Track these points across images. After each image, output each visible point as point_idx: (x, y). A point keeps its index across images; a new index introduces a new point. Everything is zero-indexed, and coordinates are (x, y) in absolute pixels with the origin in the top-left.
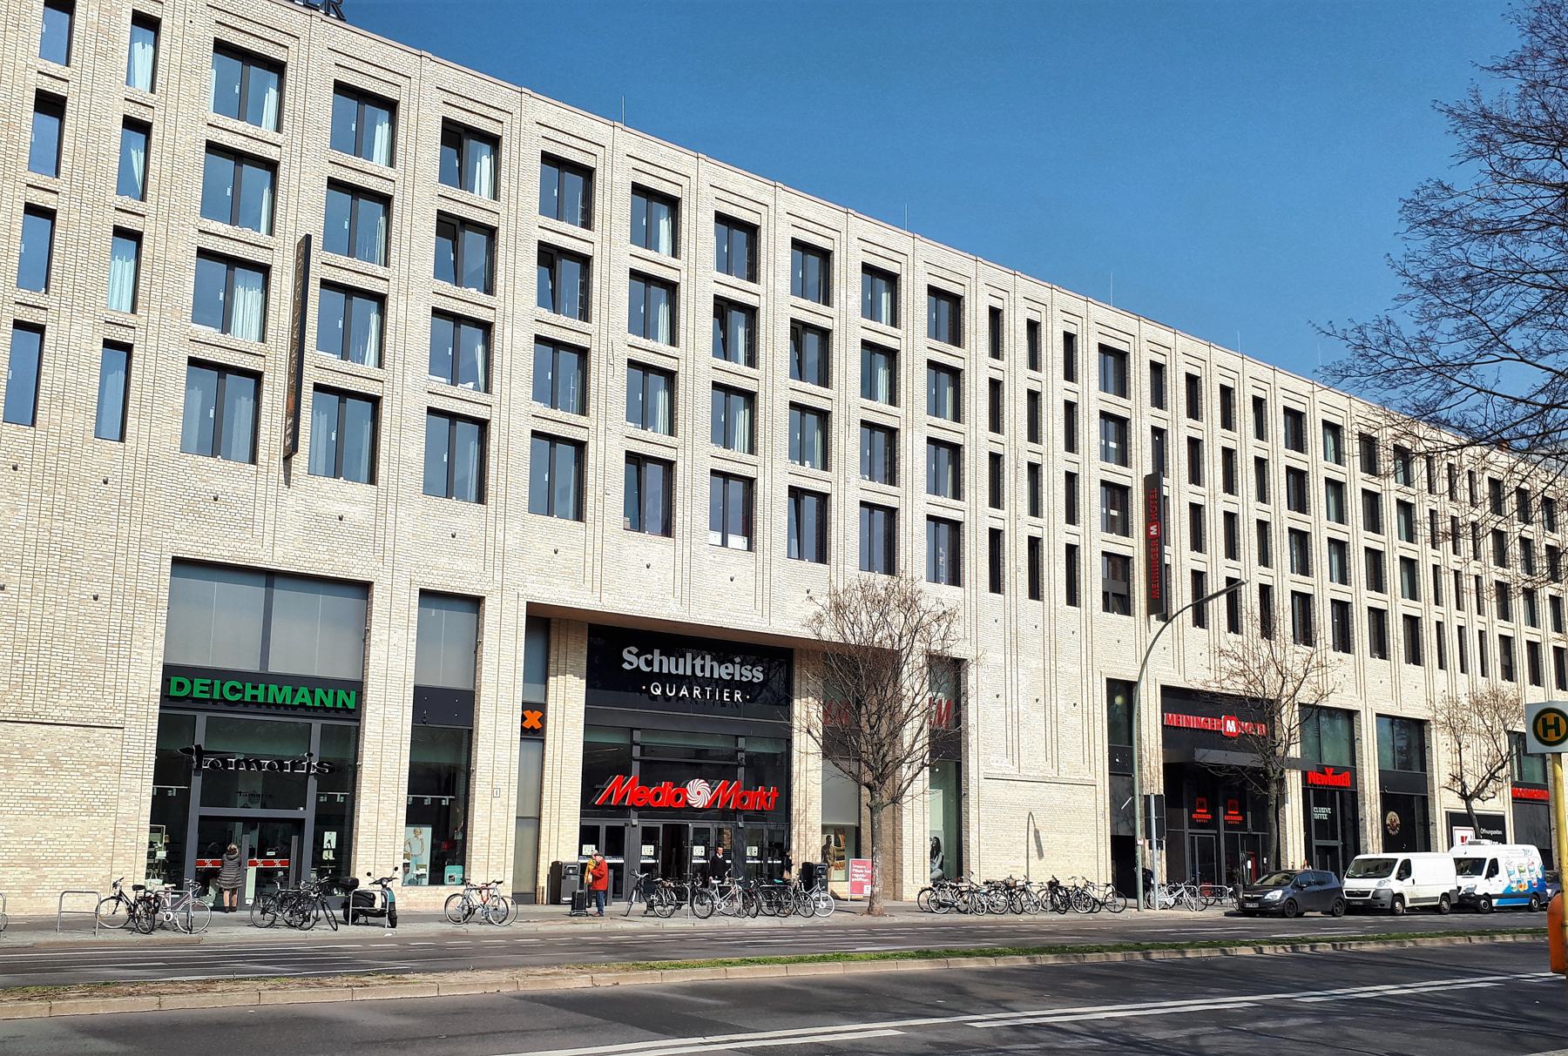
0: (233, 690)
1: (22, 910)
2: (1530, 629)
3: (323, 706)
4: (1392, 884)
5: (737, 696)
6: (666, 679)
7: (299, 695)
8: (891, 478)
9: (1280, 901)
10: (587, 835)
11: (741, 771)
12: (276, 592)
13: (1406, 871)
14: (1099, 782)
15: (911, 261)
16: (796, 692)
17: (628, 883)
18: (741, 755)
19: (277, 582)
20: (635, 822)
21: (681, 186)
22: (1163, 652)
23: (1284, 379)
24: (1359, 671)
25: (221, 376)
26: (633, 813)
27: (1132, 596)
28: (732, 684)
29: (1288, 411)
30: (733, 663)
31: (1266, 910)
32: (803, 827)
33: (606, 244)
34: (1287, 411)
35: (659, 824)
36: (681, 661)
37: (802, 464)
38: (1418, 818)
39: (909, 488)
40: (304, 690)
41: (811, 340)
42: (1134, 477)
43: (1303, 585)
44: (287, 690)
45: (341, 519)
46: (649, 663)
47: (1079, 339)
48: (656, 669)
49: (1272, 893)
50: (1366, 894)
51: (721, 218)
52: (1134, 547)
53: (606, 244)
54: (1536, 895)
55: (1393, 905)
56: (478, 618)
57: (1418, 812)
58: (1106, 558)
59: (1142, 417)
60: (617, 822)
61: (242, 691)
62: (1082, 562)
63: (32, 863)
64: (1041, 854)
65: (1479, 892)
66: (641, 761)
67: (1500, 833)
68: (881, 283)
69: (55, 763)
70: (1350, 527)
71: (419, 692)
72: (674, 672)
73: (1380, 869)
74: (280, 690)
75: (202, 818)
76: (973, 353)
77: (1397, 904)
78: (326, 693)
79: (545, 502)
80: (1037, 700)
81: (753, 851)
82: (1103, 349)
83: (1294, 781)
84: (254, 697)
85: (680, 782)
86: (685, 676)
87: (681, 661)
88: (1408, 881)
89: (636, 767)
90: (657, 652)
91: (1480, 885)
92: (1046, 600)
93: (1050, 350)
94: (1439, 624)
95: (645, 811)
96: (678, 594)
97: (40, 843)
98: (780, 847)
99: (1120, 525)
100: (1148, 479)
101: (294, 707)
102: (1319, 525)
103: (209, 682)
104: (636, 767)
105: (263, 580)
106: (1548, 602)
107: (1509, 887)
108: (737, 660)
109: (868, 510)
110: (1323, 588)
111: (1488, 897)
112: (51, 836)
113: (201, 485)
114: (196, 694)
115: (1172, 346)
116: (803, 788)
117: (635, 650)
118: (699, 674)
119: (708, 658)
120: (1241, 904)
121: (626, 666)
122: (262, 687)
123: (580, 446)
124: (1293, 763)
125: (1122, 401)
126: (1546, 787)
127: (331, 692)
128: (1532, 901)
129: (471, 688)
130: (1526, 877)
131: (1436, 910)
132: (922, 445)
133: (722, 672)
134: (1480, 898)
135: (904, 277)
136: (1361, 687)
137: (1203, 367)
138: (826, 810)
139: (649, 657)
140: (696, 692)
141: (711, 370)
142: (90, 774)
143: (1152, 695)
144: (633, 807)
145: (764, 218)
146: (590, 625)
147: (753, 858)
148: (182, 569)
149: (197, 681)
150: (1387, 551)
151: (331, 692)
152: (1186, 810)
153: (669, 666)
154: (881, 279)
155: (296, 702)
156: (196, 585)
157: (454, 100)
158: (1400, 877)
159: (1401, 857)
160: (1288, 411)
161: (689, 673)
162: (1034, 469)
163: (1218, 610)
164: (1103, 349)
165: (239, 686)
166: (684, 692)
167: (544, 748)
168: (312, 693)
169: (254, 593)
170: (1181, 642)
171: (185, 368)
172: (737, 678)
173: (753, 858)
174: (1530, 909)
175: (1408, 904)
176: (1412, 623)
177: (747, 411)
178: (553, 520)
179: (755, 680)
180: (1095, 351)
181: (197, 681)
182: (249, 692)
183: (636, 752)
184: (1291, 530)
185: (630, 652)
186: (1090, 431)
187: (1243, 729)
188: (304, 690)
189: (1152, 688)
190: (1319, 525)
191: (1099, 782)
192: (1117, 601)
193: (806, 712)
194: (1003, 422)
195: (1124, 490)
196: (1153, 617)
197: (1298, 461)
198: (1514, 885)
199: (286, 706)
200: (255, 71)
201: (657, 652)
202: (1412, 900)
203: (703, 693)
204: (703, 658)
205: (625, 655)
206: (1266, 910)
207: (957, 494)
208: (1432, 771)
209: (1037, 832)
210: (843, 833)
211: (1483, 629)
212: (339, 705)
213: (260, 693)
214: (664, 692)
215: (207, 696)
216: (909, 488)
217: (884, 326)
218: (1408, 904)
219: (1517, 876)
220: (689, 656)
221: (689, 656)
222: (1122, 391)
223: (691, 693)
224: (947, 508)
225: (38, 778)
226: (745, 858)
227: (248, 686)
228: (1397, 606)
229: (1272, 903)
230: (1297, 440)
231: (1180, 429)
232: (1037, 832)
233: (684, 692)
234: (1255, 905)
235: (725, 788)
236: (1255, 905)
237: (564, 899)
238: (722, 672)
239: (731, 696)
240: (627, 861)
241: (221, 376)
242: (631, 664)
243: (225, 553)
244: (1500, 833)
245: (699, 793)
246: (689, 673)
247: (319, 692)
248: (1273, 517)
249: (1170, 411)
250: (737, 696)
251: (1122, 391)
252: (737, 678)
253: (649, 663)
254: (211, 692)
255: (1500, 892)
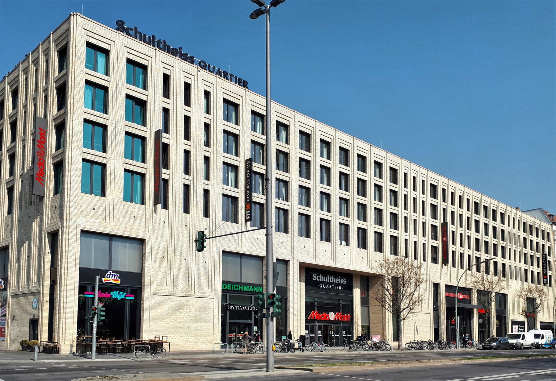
0: (236, 287)
1: (194, 349)
2: (486, 255)
3: (255, 292)
4: (520, 341)
5: (340, 288)
6: (323, 283)
7: (250, 289)
8: (308, 205)
9: (496, 345)
10: (307, 328)
11: (341, 309)
12: (113, 242)
13: (523, 338)
14: (431, 313)
15: (215, 87)
16: (354, 287)
17: (341, 341)
18: (341, 305)
19: (113, 239)
20: (317, 324)
21: (170, 70)
22: (445, 275)
23: (475, 193)
24: (449, 271)
25: (92, 165)
26: (316, 322)
27: (438, 258)
28: (338, 284)
29: (391, 169)
30: (339, 278)
31: (491, 348)
32: (356, 326)
33: (314, 157)
34: (431, 185)
35: (322, 324)
36: (326, 277)
37: (279, 199)
38: (503, 322)
39: (386, 227)
40: (251, 287)
41: (282, 156)
42: (438, 223)
43: (379, 229)
44: (248, 287)
45: (257, 239)
46: (319, 278)
47: (332, 144)
48: (321, 280)
49: (493, 344)
50: (514, 344)
51: (225, 101)
52: (438, 244)
53: (314, 157)
54: (552, 344)
55: (521, 347)
56: (143, 247)
57: (503, 320)
58: (300, 216)
59: (441, 205)
60: (313, 324)
61: (238, 288)
62: (332, 227)
63: (196, 336)
64: (418, 334)
65: (540, 343)
66: (317, 306)
67: (524, 326)
68: (232, 108)
69: (200, 308)
70: (438, 221)
71: (81, 269)
72: (325, 281)
73: (517, 337)
74: (246, 287)
75: (229, 323)
76: (400, 186)
77: (522, 347)
78: (261, 288)
79: (129, 197)
80: (205, 262)
81: (344, 332)
82: (301, 132)
83: (476, 311)
84: (241, 289)
85: (328, 312)
86: (327, 282)
87: (326, 277)
88: (524, 340)
89: (316, 308)
90: (321, 275)
91: (540, 341)
92: (332, 242)
93: (244, 116)
94: (424, 244)
95: (319, 321)
96: (332, 259)
97: (197, 330)
98: (350, 331)
99: (435, 237)
100: (442, 224)
101: (249, 292)
102: (371, 202)
103: (231, 285)
104: (316, 308)
105: (108, 238)
106: (501, 248)
107: (546, 342)
108: (340, 277)
109: (226, 198)
110: (371, 227)
111: (542, 344)
112: (200, 328)
113: (226, 230)
114: (228, 289)
115: (439, 180)
116: (356, 315)
117: (316, 275)
118: (331, 281)
119: (333, 277)
120: (483, 346)
121: (314, 279)
122: (242, 286)
123: (104, 166)
124: (475, 307)
125: (364, 174)
126: (262, 286)
127: (257, 287)
128: (551, 345)
129: (285, 286)
130: (550, 339)
131: (530, 348)
132: (297, 187)
133: (336, 281)
134: (540, 345)
135: (212, 93)
136: (291, 249)
137: (384, 160)
138: (362, 321)
139: (319, 276)
140: (330, 287)
141: (125, 126)
142: (207, 311)
143: (295, 266)
144: (317, 320)
145: (150, 62)
146: (305, 267)
147: (344, 334)
148: (85, 235)
149: (228, 285)
150: (384, 209)
151: (257, 287)
152: (450, 320)
153: (324, 279)
154: (326, 144)
155: (250, 291)
156: (230, 258)
157: (91, 34)
158: (523, 339)
159: (522, 333)
160: (391, 169)
161: (328, 281)
162: (207, 159)
163: (483, 267)
164: (301, 132)
165: (237, 286)
166: (327, 287)
167: (369, 308)
168: (253, 288)
169: (237, 260)
170: (312, 247)
171: (222, 196)
172: (340, 283)
173: (344, 334)
174: (550, 348)
175: (524, 347)
176: (394, 239)
177: (345, 205)
178: (92, 196)
179: (344, 283)
180: (297, 134)
181: (228, 285)
182: (240, 288)
183: (316, 304)
184: (375, 208)
185: (314, 275)
186: (217, 138)
187: (463, 297)
188: (251, 287)
189: (295, 263)
190: (371, 202)
191: (431, 313)
192: (435, 260)
193: (357, 293)
194: (239, 150)
195: (235, 168)
196: (443, 264)
197: (363, 176)
198: (547, 341)
199: (247, 291)
200: (137, 69)
201: (321, 275)
202: (525, 345)
203: (332, 287)
204: (332, 277)
205: (314, 276)
206: (491, 348)
207: (329, 210)
208: (508, 309)
209: (417, 327)
210: (364, 328)
211: (425, 243)
212: (259, 291)
213: (242, 288)
214: (323, 287)
215: (231, 289)
216: (386, 227)
217: (232, 125)
218: (524, 347)
219: (548, 339)
220: (328, 276)
221: (328, 276)
222: (308, 149)
223: (329, 287)
224: (305, 210)
225: (196, 312)
226: (342, 334)
227: (239, 286)
228: (387, 231)
229: (493, 346)
230: (394, 180)
231: (450, 208)
232: (417, 327)
233: (327, 287)
234: (489, 347)
235: (338, 314)
236: (489, 347)
237: (8, 348)
238: (336, 281)
239: (338, 288)
240: (315, 335)
241: (92, 165)
242: (315, 279)
243: (234, 249)
244: (524, 326)
245: (332, 316)
246: (328, 281)
247: (255, 288)
248: (384, 208)
249: (384, 180)
250: (340, 288)
251: (308, 149)
252: (340, 283)
253: (319, 278)
254: (231, 288)
255: (544, 343)
